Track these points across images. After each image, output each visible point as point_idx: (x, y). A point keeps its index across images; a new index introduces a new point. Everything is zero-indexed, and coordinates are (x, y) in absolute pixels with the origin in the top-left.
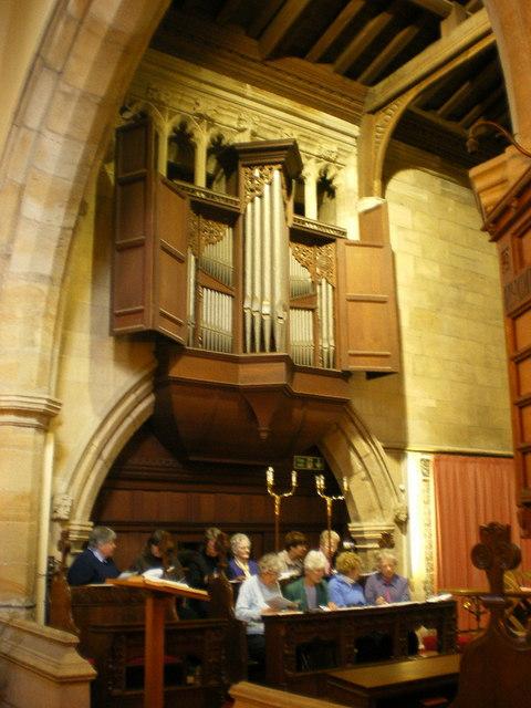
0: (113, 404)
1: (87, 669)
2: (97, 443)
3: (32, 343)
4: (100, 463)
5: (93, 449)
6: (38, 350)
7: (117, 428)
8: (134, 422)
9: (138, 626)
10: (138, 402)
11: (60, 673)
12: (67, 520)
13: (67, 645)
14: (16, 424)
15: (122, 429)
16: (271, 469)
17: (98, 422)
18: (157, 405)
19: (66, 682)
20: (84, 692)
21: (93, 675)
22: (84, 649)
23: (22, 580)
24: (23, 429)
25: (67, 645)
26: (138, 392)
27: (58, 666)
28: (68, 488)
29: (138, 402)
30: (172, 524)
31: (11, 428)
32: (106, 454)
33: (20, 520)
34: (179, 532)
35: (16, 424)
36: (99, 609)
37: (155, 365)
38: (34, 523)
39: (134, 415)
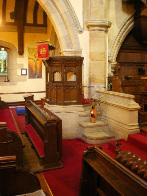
0: (123, 24)
1: (138, 106)
2: (118, 37)
3: (102, 3)
4: (119, 43)
5: (118, 39)
6: (104, 5)
7: (127, 28)
8: (128, 30)
9: (145, 93)
10: (130, 24)
11: (131, 107)
12: (111, 61)
13: (132, 98)
14: (99, 30)
15: (123, 36)
16: (30, 100)
17: (119, 30)
18: (134, 25)
19: (131, 110)
20: (136, 114)
21: (139, 108)
22: (136, 100)
23: (103, 79)
24: (102, 31)
25: (132, 98)
26: (130, 20)
27: (129, 105)
28: (111, 51)
29: (130, 24)
30: (138, 63)
31: (97, 31)
32: (121, 41)
33: (102, 61)
34: (139, 65)
35: (99, 30)
36: (127, 87)
37: (135, 12)
38: (105, 62)
39: (128, 28)
